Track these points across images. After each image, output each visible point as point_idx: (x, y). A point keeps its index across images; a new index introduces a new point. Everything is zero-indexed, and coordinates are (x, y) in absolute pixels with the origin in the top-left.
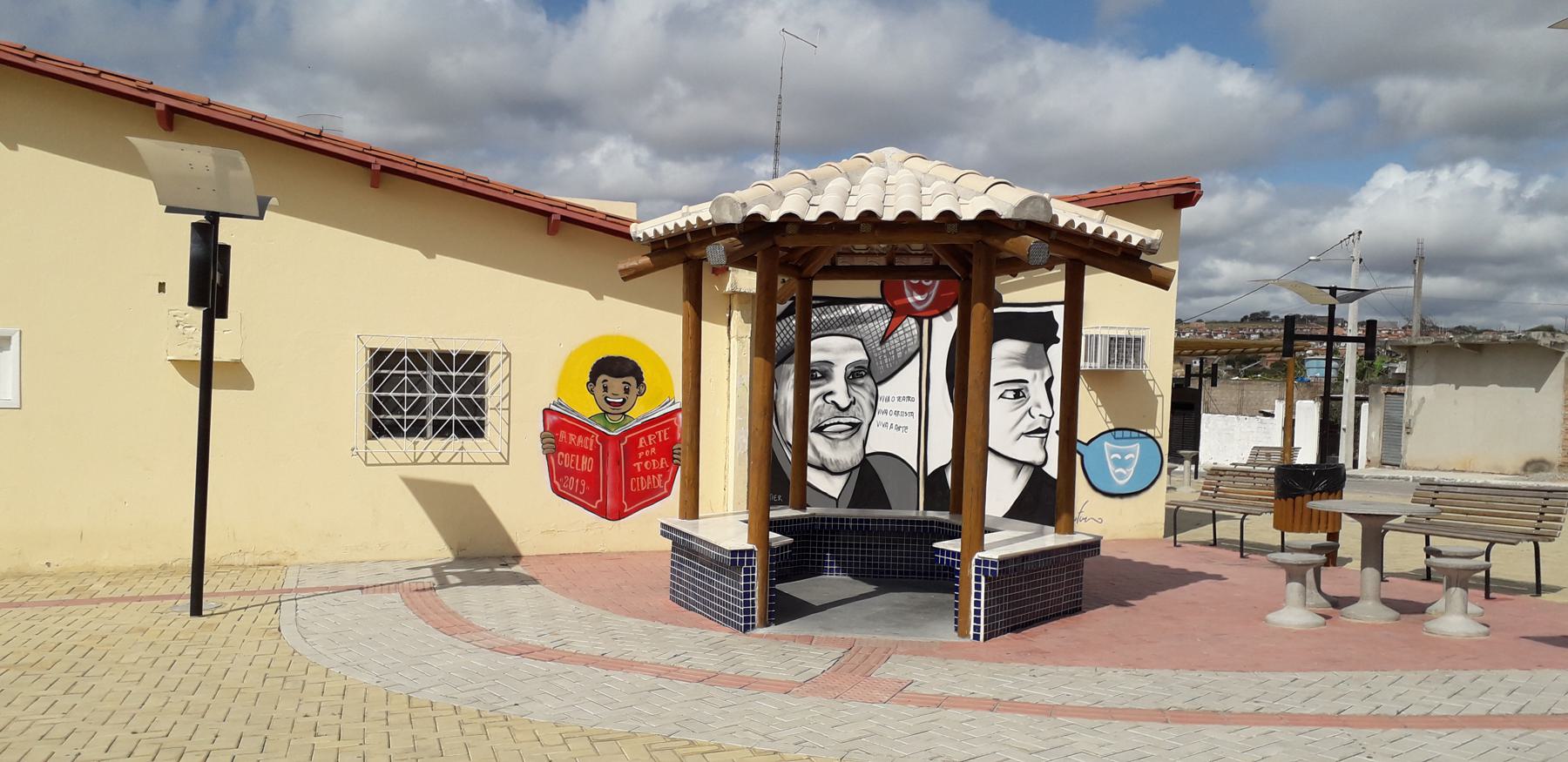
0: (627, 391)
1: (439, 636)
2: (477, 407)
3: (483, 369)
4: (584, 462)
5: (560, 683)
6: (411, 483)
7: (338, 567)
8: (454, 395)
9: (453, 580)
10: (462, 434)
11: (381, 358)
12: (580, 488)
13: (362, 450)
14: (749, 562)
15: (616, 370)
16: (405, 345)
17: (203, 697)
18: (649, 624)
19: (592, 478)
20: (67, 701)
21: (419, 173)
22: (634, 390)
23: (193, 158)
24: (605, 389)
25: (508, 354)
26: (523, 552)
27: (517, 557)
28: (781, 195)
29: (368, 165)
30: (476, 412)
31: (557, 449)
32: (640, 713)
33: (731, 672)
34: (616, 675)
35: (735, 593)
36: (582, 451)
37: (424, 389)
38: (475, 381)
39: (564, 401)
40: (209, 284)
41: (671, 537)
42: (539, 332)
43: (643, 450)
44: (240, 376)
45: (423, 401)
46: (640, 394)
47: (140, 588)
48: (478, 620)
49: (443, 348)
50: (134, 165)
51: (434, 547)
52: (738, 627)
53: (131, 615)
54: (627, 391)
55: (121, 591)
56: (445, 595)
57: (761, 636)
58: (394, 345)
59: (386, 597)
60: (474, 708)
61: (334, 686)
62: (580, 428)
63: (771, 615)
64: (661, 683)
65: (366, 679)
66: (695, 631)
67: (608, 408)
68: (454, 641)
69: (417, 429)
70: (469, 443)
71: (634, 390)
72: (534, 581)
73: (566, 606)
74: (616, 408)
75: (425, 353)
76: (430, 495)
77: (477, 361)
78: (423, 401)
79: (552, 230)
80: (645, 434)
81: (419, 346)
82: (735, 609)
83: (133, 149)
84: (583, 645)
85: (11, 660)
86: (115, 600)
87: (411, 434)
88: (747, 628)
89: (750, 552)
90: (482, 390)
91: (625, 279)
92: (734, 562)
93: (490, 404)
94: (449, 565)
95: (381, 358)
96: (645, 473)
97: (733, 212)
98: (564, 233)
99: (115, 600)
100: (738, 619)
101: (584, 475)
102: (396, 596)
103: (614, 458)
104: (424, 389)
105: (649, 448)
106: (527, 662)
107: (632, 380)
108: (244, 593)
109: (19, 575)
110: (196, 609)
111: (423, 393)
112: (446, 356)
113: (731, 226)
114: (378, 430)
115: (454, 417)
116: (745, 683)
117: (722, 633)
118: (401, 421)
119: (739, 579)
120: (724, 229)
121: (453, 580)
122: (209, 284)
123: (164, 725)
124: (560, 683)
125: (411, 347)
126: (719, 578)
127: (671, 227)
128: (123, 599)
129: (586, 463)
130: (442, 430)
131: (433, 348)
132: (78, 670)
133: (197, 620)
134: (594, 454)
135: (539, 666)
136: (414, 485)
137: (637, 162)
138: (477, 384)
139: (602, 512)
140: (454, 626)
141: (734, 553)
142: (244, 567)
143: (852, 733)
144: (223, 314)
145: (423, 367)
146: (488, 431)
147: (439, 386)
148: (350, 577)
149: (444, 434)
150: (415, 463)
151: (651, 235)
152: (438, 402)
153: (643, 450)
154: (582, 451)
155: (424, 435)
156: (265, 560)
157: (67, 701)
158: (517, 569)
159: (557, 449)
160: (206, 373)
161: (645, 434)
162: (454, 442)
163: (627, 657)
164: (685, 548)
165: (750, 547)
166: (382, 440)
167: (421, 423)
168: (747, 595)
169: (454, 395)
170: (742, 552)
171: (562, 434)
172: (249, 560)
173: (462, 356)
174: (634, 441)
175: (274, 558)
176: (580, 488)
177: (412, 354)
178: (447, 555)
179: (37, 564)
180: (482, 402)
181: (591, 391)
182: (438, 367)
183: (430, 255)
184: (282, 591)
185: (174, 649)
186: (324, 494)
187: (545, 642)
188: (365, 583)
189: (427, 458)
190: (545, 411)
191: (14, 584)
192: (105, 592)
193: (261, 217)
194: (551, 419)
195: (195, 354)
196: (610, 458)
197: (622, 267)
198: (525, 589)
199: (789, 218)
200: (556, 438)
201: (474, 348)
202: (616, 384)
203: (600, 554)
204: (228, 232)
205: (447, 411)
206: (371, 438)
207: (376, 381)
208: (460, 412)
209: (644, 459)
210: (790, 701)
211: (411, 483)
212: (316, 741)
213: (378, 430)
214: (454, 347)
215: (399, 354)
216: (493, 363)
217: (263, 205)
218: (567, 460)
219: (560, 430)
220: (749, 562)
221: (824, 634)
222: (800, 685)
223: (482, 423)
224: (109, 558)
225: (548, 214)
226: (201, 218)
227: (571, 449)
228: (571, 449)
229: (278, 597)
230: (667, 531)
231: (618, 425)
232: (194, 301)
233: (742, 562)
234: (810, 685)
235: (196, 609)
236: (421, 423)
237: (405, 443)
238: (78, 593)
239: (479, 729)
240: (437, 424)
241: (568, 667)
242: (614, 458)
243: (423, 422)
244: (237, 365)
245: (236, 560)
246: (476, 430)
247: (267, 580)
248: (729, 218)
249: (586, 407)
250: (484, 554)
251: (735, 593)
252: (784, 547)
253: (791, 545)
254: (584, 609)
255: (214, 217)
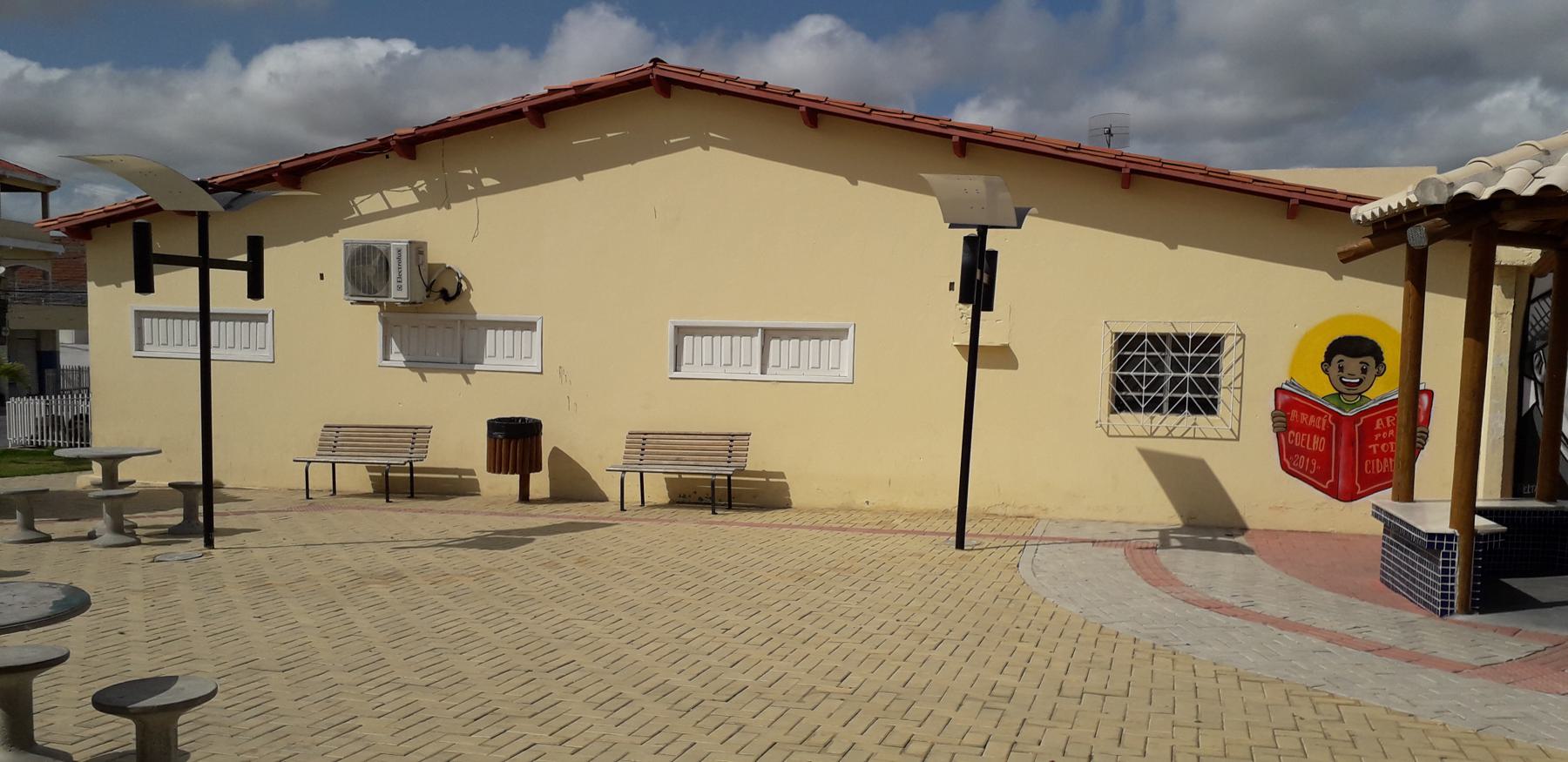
0: (1364, 371)
1: (1146, 585)
2: (1211, 386)
3: (1218, 350)
4: (1315, 442)
5: (1234, 634)
6: (1148, 455)
7: (1080, 523)
8: (1188, 374)
9: (1174, 542)
10: (1194, 411)
11: (1125, 342)
12: (1311, 466)
13: (1105, 423)
14: (1449, 547)
15: (1352, 349)
16: (1146, 330)
17: (949, 605)
18: (1345, 599)
19: (1324, 459)
20: (861, 595)
21: (1164, 172)
22: (1372, 370)
23: (971, 184)
24: (1341, 369)
25: (1243, 336)
26: (1250, 525)
27: (1244, 529)
28: (1500, 171)
29: (1119, 169)
30: (1209, 391)
31: (1288, 428)
32: (1295, 667)
33: (1406, 647)
34: (1287, 635)
35: (1435, 577)
36: (1313, 431)
37: (1161, 368)
38: (1209, 361)
39: (1297, 381)
40: (977, 285)
41: (1381, 519)
42: (1277, 315)
43: (1381, 431)
44: (1005, 357)
45: (1160, 380)
46: (1380, 374)
47: (926, 525)
48: (1183, 577)
49: (1181, 330)
50: (926, 189)
51: (1163, 512)
52: (1434, 611)
53: (914, 544)
54: (1364, 371)
55: (913, 526)
56: (1164, 556)
57: (1459, 623)
58: (1136, 329)
59: (1112, 551)
60: (1151, 641)
61: (1046, 610)
62: (1313, 408)
63: (1474, 603)
64: (1328, 647)
65: (1073, 609)
66: (1389, 611)
67: (1343, 389)
68: (1156, 591)
69: (1153, 406)
70: (1202, 419)
71: (1372, 370)
72: (1249, 551)
73: (1271, 574)
74: (1354, 389)
75: (1164, 336)
76: (1161, 465)
77: (1212, 343)
78: (1160, 380)
79: (1292, 214)
80: (1383, 416)
81: (1158, 329)
82: (1433, 593)
83: (925, 182)
84: (1269, 608)
85: (834, 564)
86: (907, 532)
87: (1148, 409)
88: (1444, 613)
89: (1450, 537)
90: (1216, 370)
91: (1344, 261)
92: (1431, 545)
93: (1223, 383)
94: (1176, 531)
95: (1125, 342)
96: (1381, 455)
97: (1438, 193)
98: (1298, 219)
99: (907, 532)
100: (1435, 602)
101: (1315, 455)
102: (1120, 551)
103: (1344, 440)
104: (1161, 368)
105: (1387, 430)
106: (1213, 615)
107: (1371, 360)
108: (1000, 536)
109: (849, 509)
110: (960, 544)
111: (1163, 373)
112: (1183, 338)
113: (1440, 206)
114: (1119, 405)
115: (1188, 394)
116: (1415, 658)
117: (1415, 615)
118: (1140, 398)
119: (1437, 562)
120: (1433, 210)
121: (1174, 542)
122: (977, 285)
123: (918, 618)
124: (1234, 634)
125: (1151, 331)
126: (1421, 561)
127: (1385, 209)
128: (913, 532)
129: (1317, 443)
130: (1178, 408)
131: (1171, 331)
132: (874, 576)
133: (960, 552)
134: (1327, 434)
135: (1220, 619)
136: (1151, 457)
137: (1533, 106)
138: (1212, 365)
139: (1333, 492)
140: (1161, 579)
141: (1431, 536)
142: (1006, 517)
143: (1505, 712)
144: (989, 308)
145: (1161, 349)
146: (1221, 409)
147: (1175, 367)
148: (1089, 532)
149: (1178, 410)
150: (1151, 436)
151: (1369, 217)
152: (1174, 381)
153: (1381, 431)
154: (1313, 431)
155: (1160, 411)
156: (1022, 512)
157: (861, 595)
158: (1240, 540)
159: (1288, 428)
160: (973, 352)
161: (1383, 416)
162: (1188, 419)
163: (1307, 622)
164: (1397, 533)
165: (1450, 531)
166: (1123, 414)
167: (1157, 400)
168: (1445, 580)
169: (1188, 374)
170: (1441, 536)
171: (1294, 413)
172: (1010, 511)
173: (1198, 338)
174: (1372, 421)
175: (1029, 512)
176: (1311, 466)
177: (1152, 337)
178: (1177, 521)
179: (860, 501)
180: (1215, 381)
181: (1326, 371)
182: (1175, 349)
183: (1172, 246)
184: (1030, 538)
185: (938, 570)
186: (1071, 457)
187: (1237, 602)
188: (1098, 538)
189: (1162, 432)
190: (1278, 391)
191: (844, 515)
192: (902, 526)
193: (1019, 226)
194: (1283, 398)
195: (966, 340)
196: (1343, 440)
197: (1341, 249)
198: (1239, 557)
199: (1503, 196)
200: (1288, 417)
201: (1210, 330)
202: (1353, 365)
203: (1329, 533)
204: (993, 240)
205: (1182, 389)
206: (1113, 412)
207: (1119, 362)
208: (1194, 390)
209: (1381, 441)
210: (1454, 679)
211: (1148, 455)
212: (1019, 645)
213: (1119, 405)
214: (1191, 330)
215: (1141, 337)
216: (1227, 345)
217: (1021, 216)
218: (1298, 438)
219: (1291, 409)
220: (1449, 547)
221: (1533, 629)
222: (1476, 668)
223: (1215, 401)
224: (908, 501)
225: (1287, 199)
226: (974, 232)
227: (1302, 428)
228: (1302, 428)
229: (1024, 542)
230: (1378, 513)
231: (1354, 405)
232: (964, 299)
233: (1440, 546)
234: (1489, 669)
235: (960, 544)
236: (1157, 400)
237: (1143, 418)
238: (884, 524)
239: (1147, 657)
240: (1172, 401)
241: (1248, 624)
242: (1344, 440)
243: (1160, 399)
244: (1005, 349)
245: (999, 511)
246: (1209, 408)
247: (1020, 528)
248: (1434, 199)
249: (1320, 386)
250: (1210, 521)
251: (1435, 577)
252: (1493, 535)
253: (1503, 533)
254: (1286, 579)
255: (983, 230)
